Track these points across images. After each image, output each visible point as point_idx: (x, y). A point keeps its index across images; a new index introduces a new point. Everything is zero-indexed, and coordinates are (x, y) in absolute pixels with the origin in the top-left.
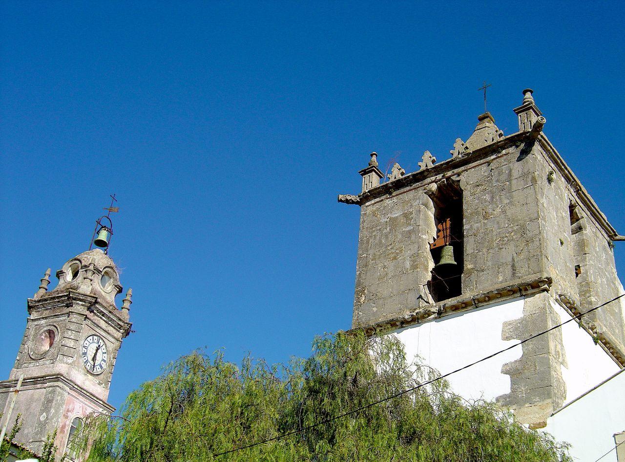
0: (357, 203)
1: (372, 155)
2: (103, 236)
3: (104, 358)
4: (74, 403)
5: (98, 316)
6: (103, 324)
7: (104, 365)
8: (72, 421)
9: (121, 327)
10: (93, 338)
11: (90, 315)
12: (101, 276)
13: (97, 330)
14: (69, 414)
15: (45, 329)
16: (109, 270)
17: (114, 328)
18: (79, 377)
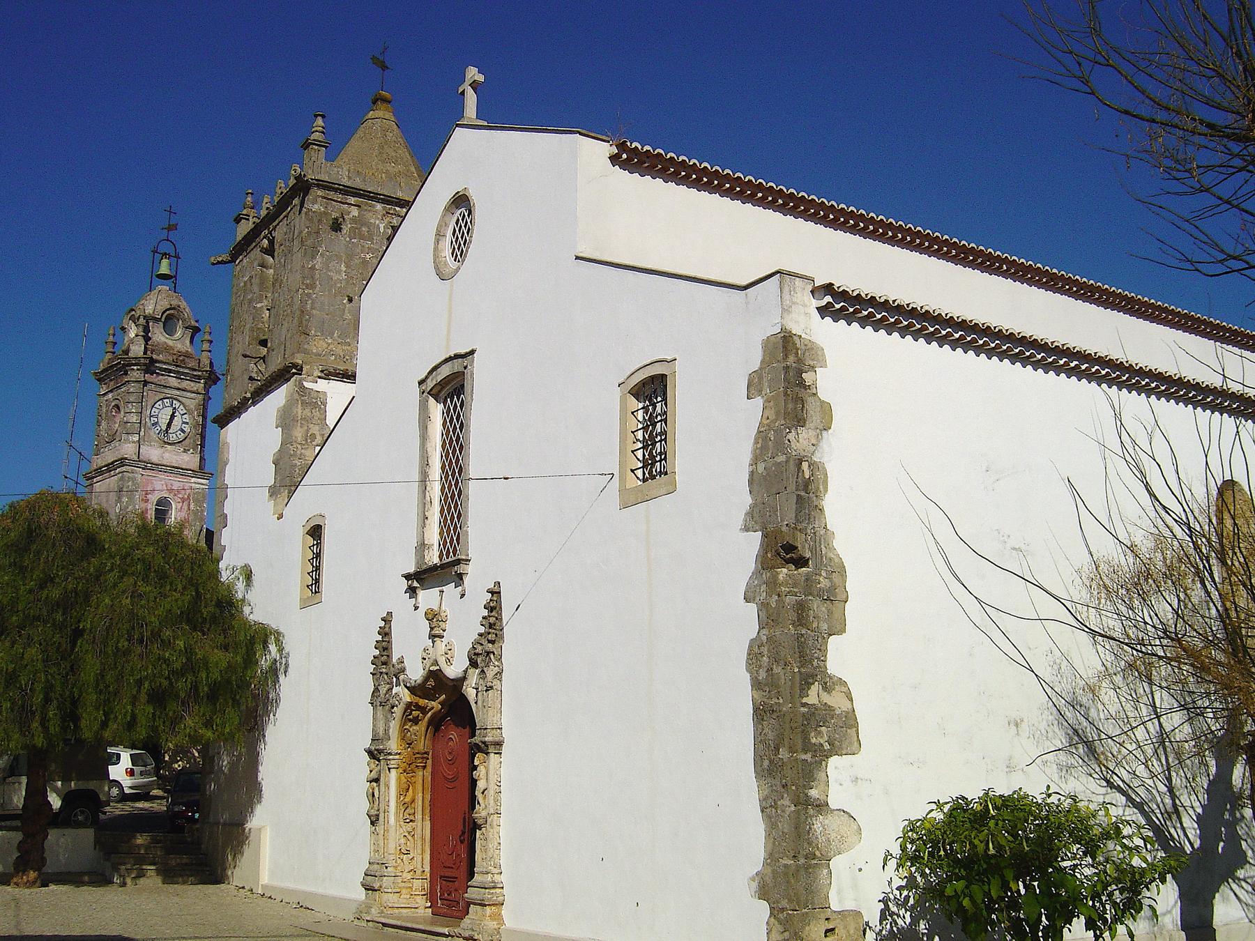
0: (229, 262)
1: (316, 116)
2: (164, 268)
3: (184, 420)
4: (152, 483)
5: (163, 375)
6: (173, 381)
7: (187, 429)
8: (155, 504)
9: (199, 377)
10: (163, 402)
11: (153, 378)
12: (161, 324)
13: (166, 391)
14: (149, 496)
15: (113, 404)
16: (172, 312)
17: (191, 381)
18: (153, 453)
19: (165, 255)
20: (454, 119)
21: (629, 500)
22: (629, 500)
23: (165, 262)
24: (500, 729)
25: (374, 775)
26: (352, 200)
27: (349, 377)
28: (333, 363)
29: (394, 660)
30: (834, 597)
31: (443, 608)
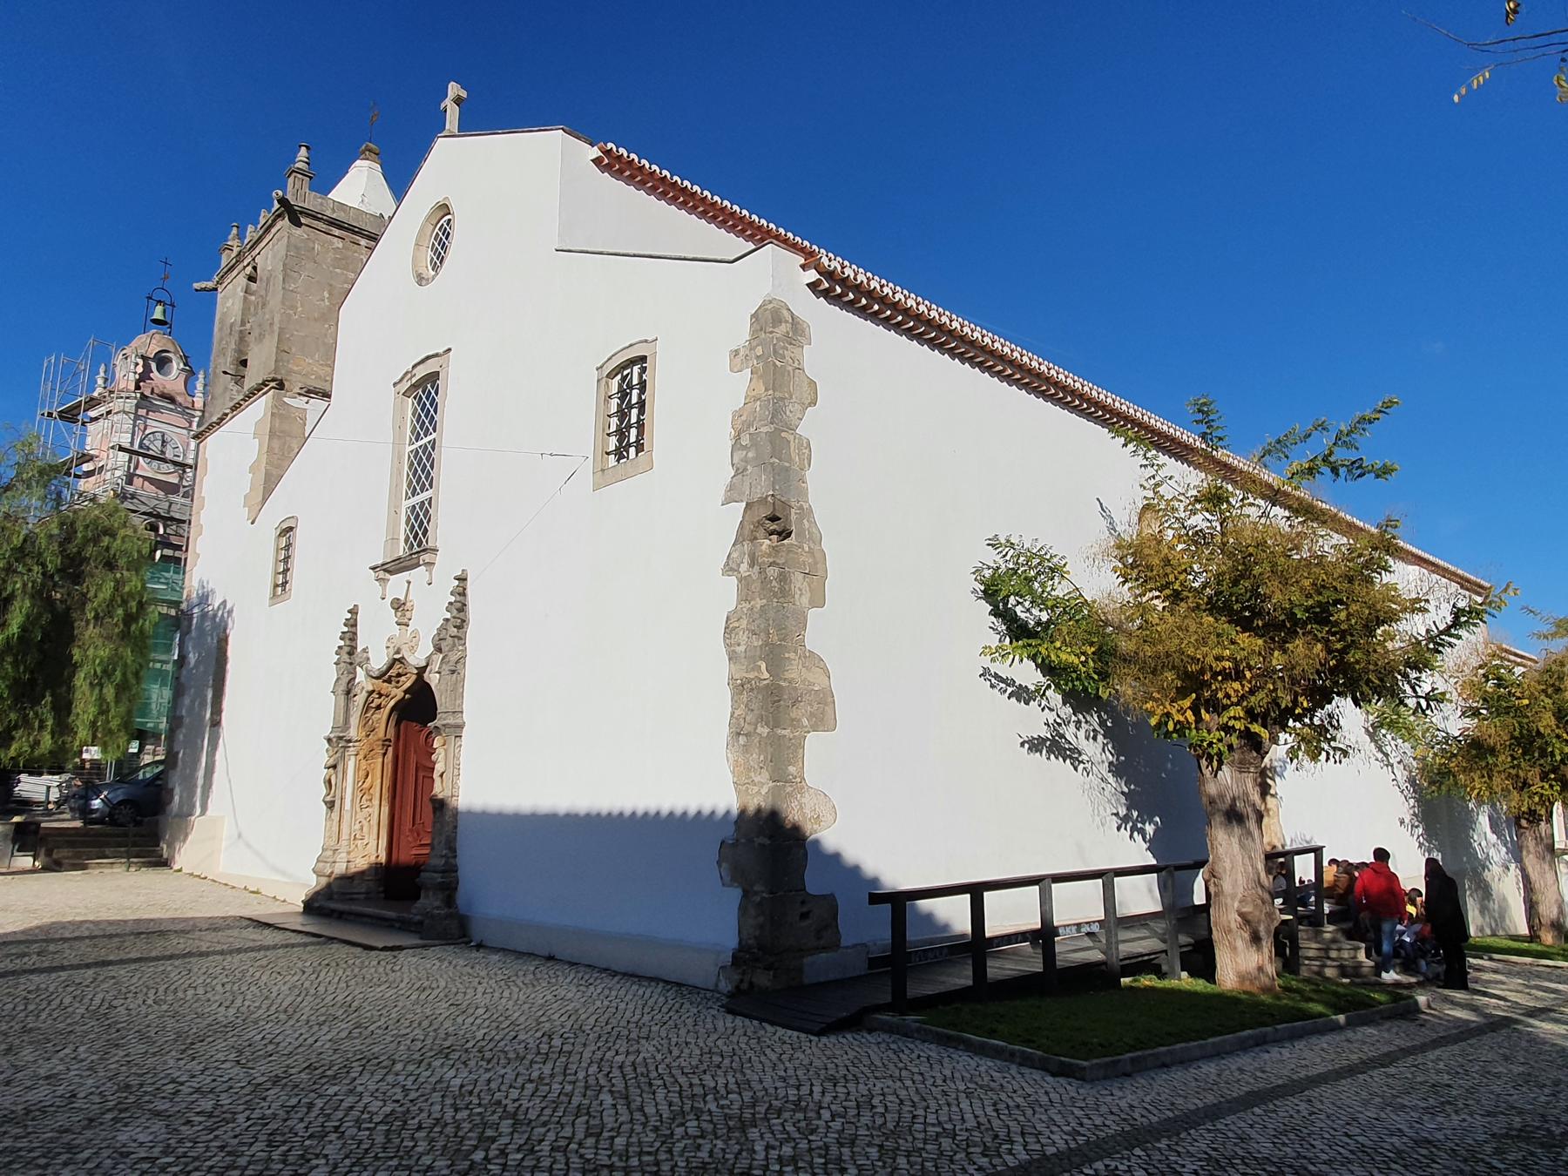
1: (300, 146)
2: (158, 313)
19: (159, 302)
20: (436, 126)
21: (603, 477)
22: (603, 477)
23: (159, 309)
24: (462, 712)
25: (331, 762)
26: (337, 232)
27: (326, 395)
28: (313, 383)
29: (359, 650)
30: (816, 572)
31: (410, 597)
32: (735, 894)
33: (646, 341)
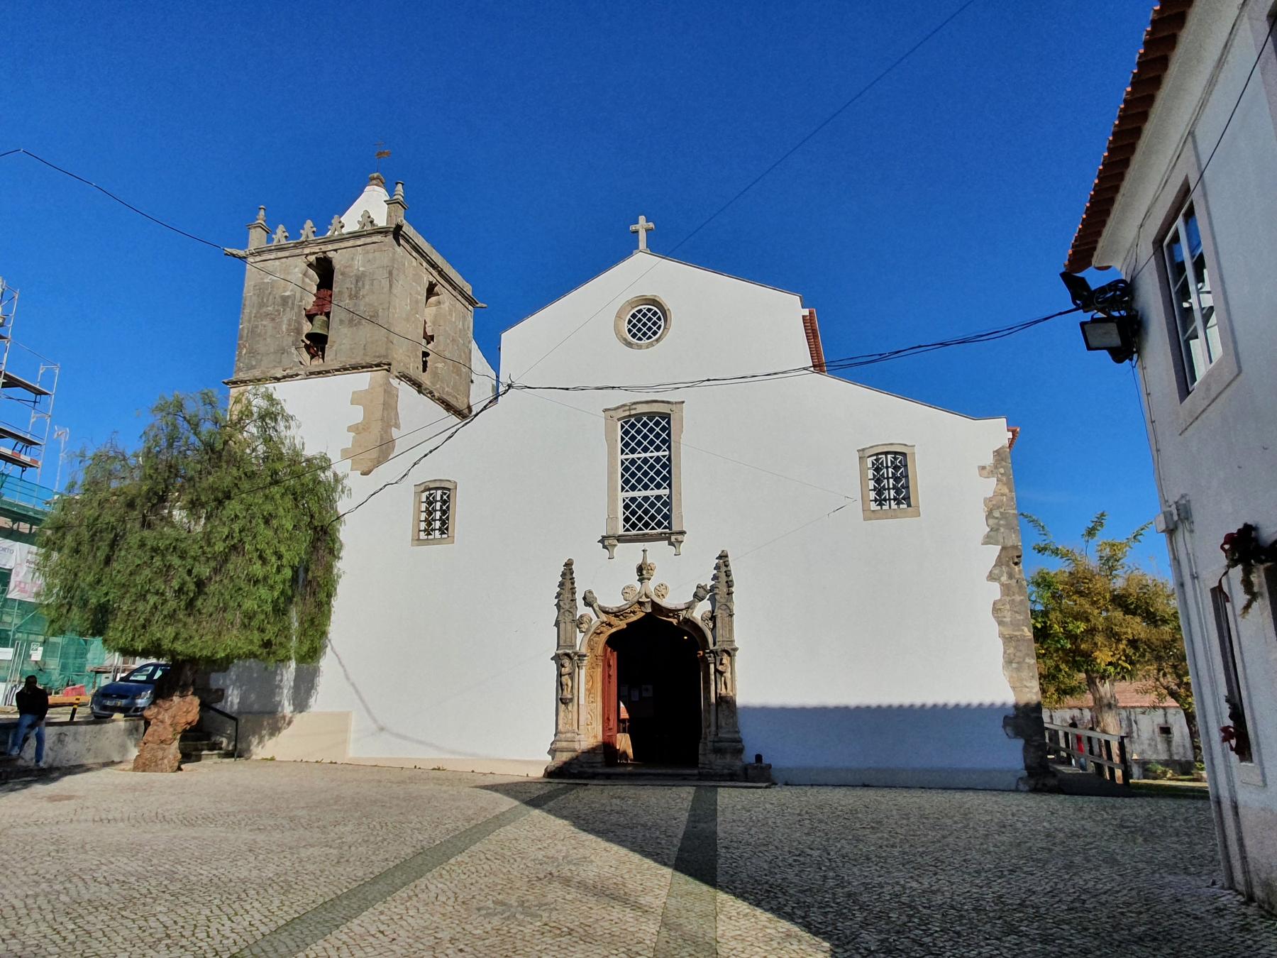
1: (397, 183)
26: (414, 254)
32: (1020, 743)
33: (905, 445)
